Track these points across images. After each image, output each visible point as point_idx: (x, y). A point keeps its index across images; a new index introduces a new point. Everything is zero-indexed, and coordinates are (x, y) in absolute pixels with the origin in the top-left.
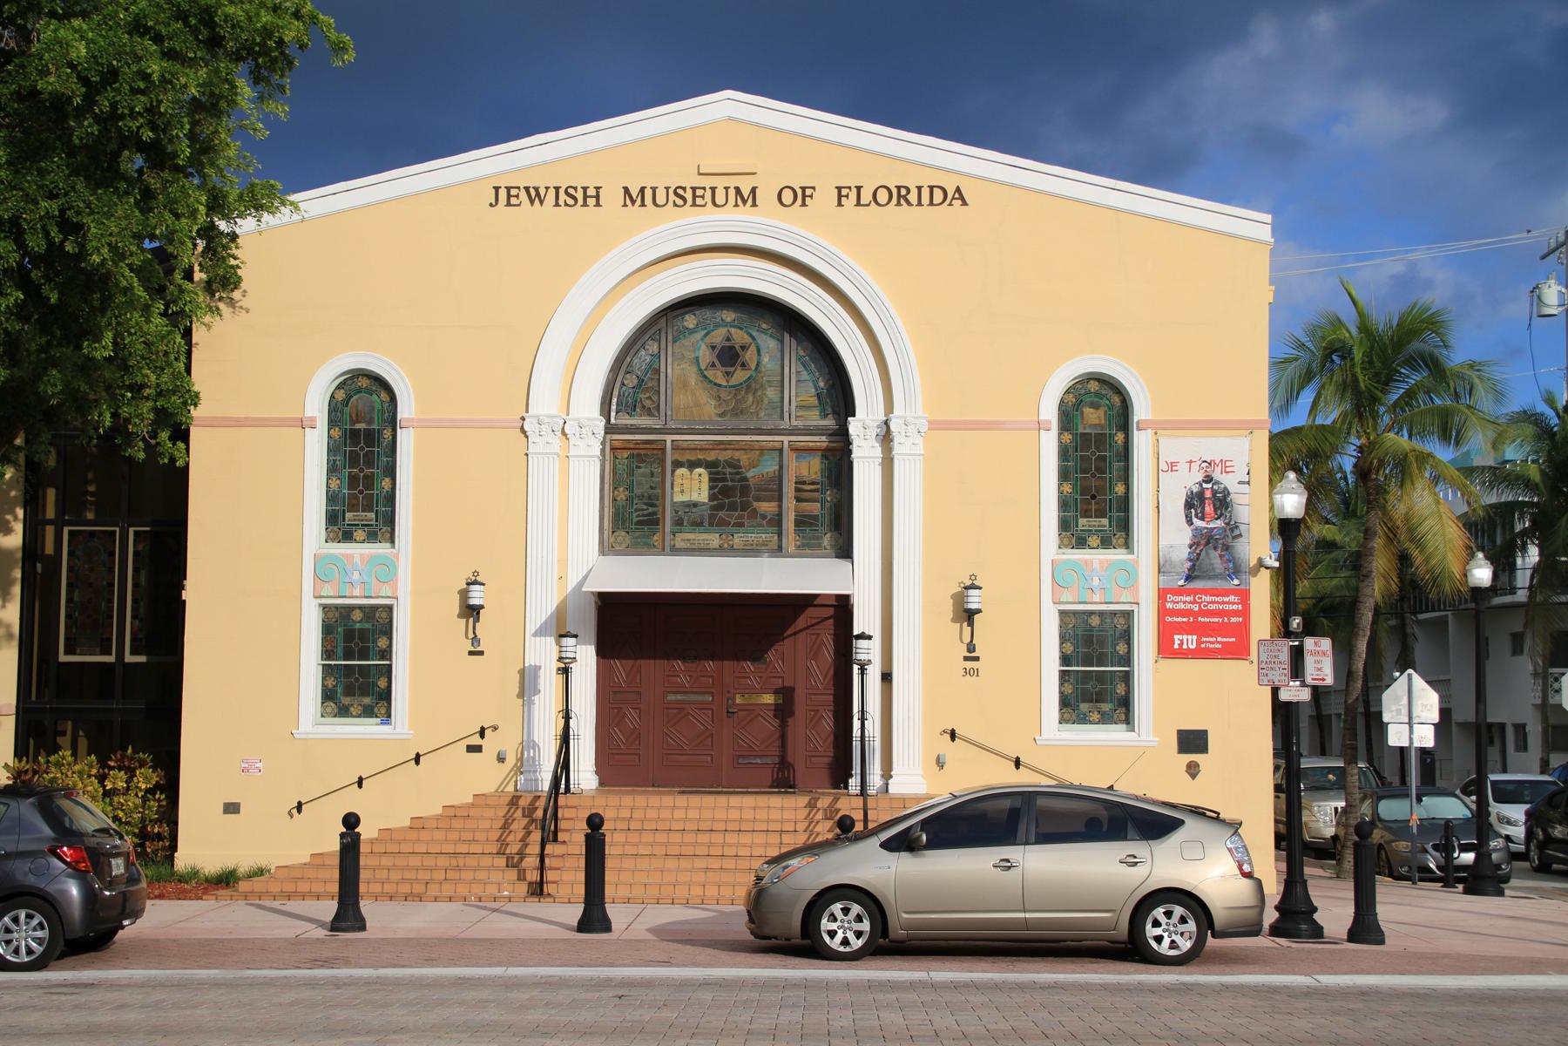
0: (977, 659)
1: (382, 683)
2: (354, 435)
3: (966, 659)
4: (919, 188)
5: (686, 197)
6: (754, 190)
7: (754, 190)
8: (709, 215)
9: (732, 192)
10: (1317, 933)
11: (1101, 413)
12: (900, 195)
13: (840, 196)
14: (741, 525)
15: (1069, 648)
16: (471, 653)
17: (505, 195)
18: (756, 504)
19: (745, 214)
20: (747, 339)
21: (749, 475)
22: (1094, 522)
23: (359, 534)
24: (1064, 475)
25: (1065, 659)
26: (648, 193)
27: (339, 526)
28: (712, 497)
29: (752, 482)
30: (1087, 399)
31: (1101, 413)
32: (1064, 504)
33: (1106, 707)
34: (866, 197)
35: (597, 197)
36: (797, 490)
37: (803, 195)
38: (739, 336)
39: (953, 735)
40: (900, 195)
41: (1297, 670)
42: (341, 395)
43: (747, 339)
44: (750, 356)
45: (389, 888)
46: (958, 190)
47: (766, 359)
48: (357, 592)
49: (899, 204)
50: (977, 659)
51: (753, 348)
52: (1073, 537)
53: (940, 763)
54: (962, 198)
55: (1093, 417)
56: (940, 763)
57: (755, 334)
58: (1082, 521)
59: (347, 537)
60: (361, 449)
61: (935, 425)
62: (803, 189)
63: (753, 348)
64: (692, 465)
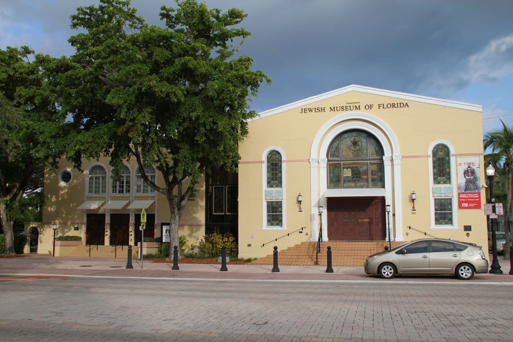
1: (280, 218)
2: (273, 164)
6: (359, 106)
7: (359, 106)
10: (501, 272)
12: (393, 105)
15: (437, 207)
19: (358, 112)
22: (442, 178)
24: (434, 167)
25: (436, 210)
27: (270, 184)
28: (352, 175)
32: (434, 174)
33: (446, 221)
34: (385, 106)
37: (371, 107)
38: (357, 139)
39: (410, 228)
40: (393, 105)
41: (494, 211)
42: (270, 156)
44: (360, 143)
52: (436, 181)
55: (441, 154)
58: (439, 178)
59: (272, 186)
60: (274, 167)
61: (403, 157)
64: (347, 168)
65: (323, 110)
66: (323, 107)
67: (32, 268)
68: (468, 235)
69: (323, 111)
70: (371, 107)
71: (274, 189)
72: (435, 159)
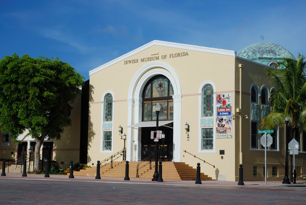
0: (189, 138)
2: (109, 103)
3: (188, 138)
4: (181, 53)
5: (149, 59)
6: (158, 57)
7: (158, 57)
8: (152, 62)
9: (155, 57)
11: (210, 91)
12: (179, 55)
13: (170, 56)
14: (162, 115)
15: (204, 135)
16: (121, 139)
17: (126, 62)
18: (164, 111)
19: (157, 61)
20: (163, 82)
21: (163, 106)
23: (209, 115)
26: (144, 59)
29: (163, 108)
30: (208, 89)
31: (210, 91)
34: (174, 56)
35: (138, 61)
36: (170, 108)
37: (165, 57)
38: (162, 82)
39: (185, 152)
40: (179, 55)
43: (163, 82)
44: (163, 85)
45: (81, 175)
46: (187, 53)
47: (166, 86)
48: (207, 126)
49: (178, 56)
50: (189, 138)
51: (164, 84)
53: (184, 156)
54: (187, 54)
56: (184, 156)
57: (164, 81)
58: (207, 111)
59: (207, 116)
60: (109, 106)
61: (126, 100)
62: (165, 55)
63: (164, 84)
65: (142, 60)
66: (137, 59)
67: (111, 201)
68: (222, 158)
69: (157, 59)
70: (165, 57)
71: (107, 122)
72: (205, 96)
